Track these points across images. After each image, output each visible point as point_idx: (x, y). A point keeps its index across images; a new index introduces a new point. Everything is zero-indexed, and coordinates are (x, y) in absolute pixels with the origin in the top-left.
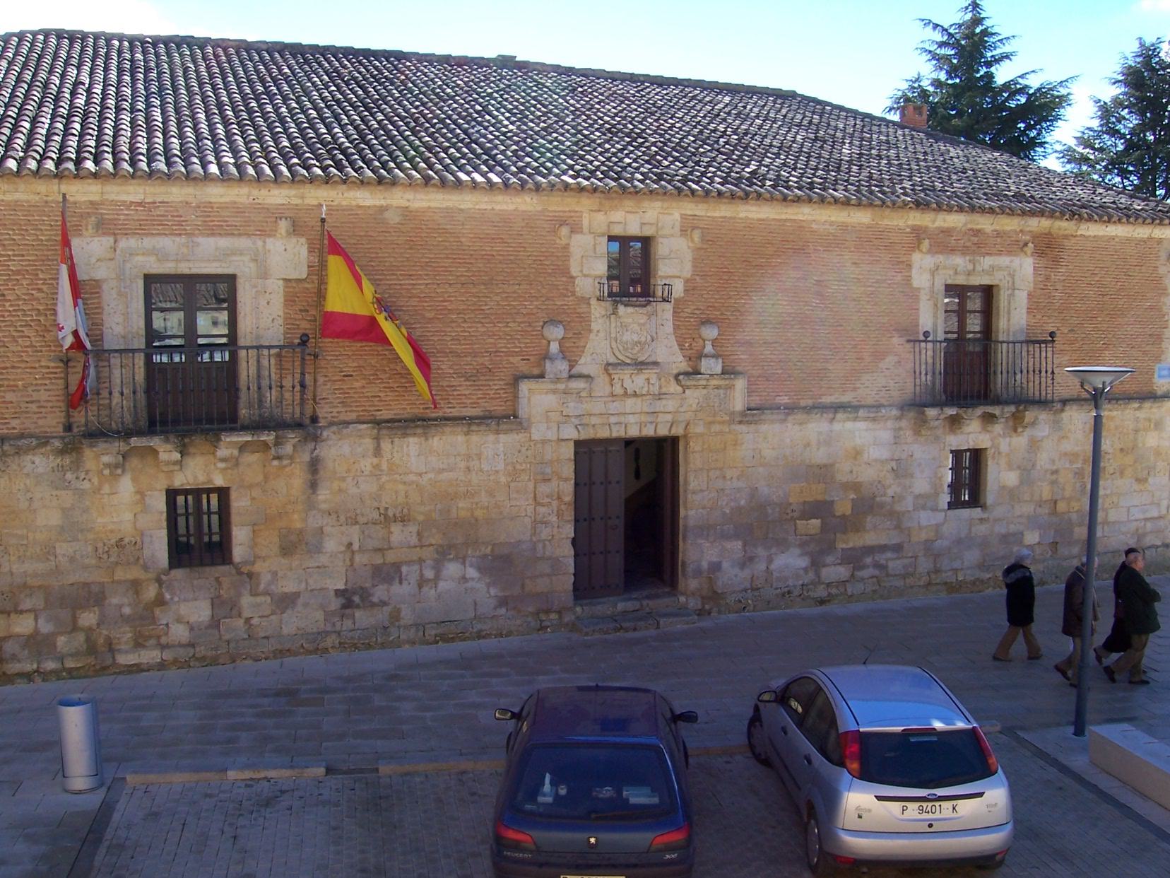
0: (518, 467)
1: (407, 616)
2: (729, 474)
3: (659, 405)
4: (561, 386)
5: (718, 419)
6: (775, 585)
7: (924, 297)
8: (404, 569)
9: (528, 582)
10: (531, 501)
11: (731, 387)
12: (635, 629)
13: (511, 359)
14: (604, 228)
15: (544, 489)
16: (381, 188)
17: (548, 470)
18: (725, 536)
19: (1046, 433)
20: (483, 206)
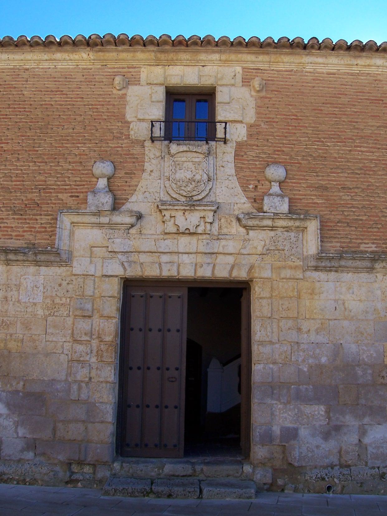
0: (57, 300)
2: (305, 326)
3: (217, 246)
4: (105, 220)
5: (290, 263)
6: (370, 464)
9: (60, 425)
10: (68, 338)
11: (304, 229)
12: (170, 496)
13: (60, 196)
14: (161, 80)
15: (84, 325)
17: (89, 306)
18: (300, 397)
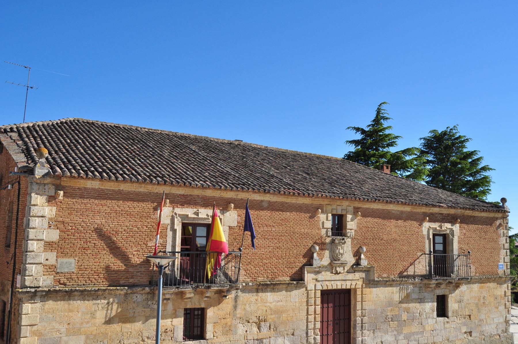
8: (264, 340)
16: (125, 183)
20: (293, 202)
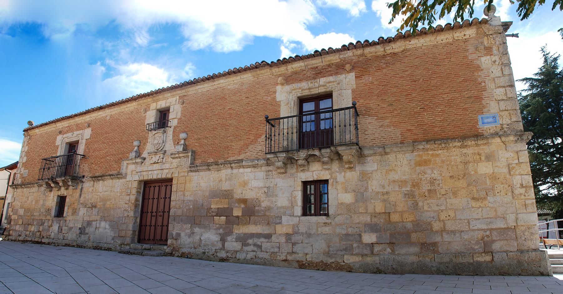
1: (91, 238)
7: (282, 105)
19: (376, 168)
